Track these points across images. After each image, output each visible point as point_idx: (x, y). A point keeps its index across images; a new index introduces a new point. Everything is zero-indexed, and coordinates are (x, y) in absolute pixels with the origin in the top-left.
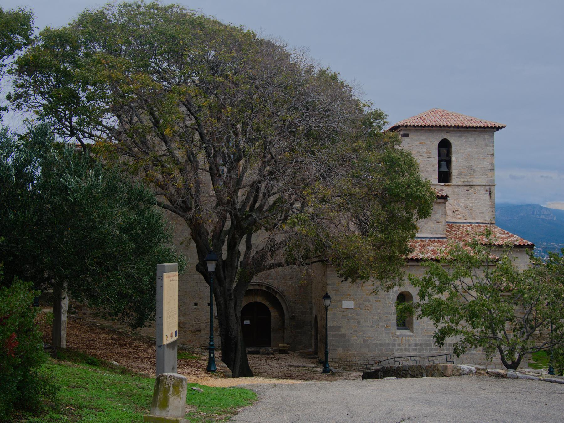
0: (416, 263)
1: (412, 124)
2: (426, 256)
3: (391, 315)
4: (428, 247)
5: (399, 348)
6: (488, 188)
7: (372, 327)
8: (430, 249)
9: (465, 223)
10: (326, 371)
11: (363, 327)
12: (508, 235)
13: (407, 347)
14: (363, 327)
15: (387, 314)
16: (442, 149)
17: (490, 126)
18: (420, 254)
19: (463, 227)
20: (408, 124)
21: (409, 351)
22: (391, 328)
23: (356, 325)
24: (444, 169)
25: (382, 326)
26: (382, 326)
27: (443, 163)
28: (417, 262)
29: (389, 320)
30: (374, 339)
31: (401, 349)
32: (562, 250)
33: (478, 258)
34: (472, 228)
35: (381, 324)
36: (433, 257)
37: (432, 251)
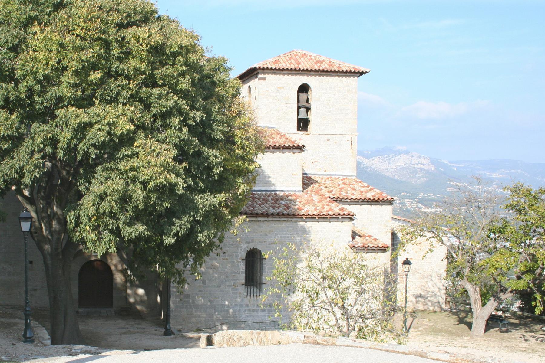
0: (266, 219)
1: (270, 67)
2: (278, 210)
3: (239, 273)
4: (281, 201)
5: (247, 308)
6: (349, 138)
7: (219, 287)
8: (284, 203)
9: (325, 175)
10: (168, 333)
11: (208, 286)
12: (368, 189)
13: (255, 308)
14: (208, 286)
15: (235, 273)
16: (300, 94)
17: (353, 70)
18: (271, 209)
19: (322, 179)
20: (266, 67)
21: (257, 312)
22: (239, 288)
23: (201, 284)
24: (303, 115)
25: (229, 286)
26: (229, 286)
27: (303, 110)
28: (267, 217)
29: (237, 280)
30: (220, 299)
31: (249, 310)
32: (82, 1)
33: (178, 222)
34: (332, 180)
35: (228, 283)
36: (285, 212)
37: (285, 205)
